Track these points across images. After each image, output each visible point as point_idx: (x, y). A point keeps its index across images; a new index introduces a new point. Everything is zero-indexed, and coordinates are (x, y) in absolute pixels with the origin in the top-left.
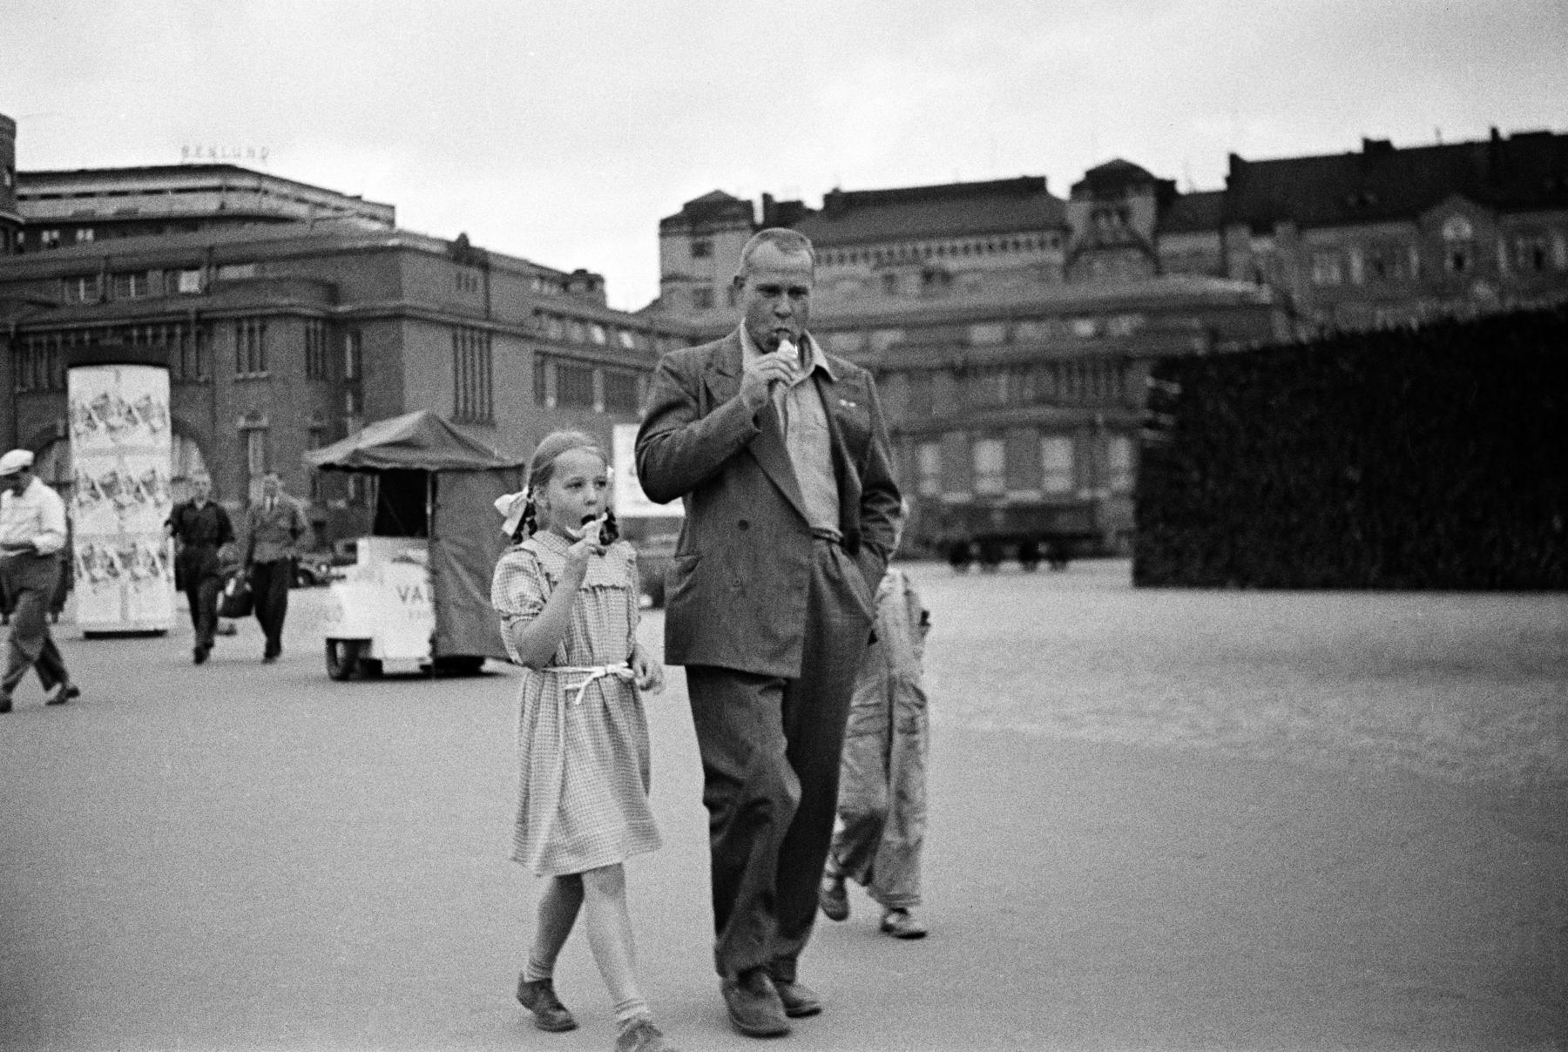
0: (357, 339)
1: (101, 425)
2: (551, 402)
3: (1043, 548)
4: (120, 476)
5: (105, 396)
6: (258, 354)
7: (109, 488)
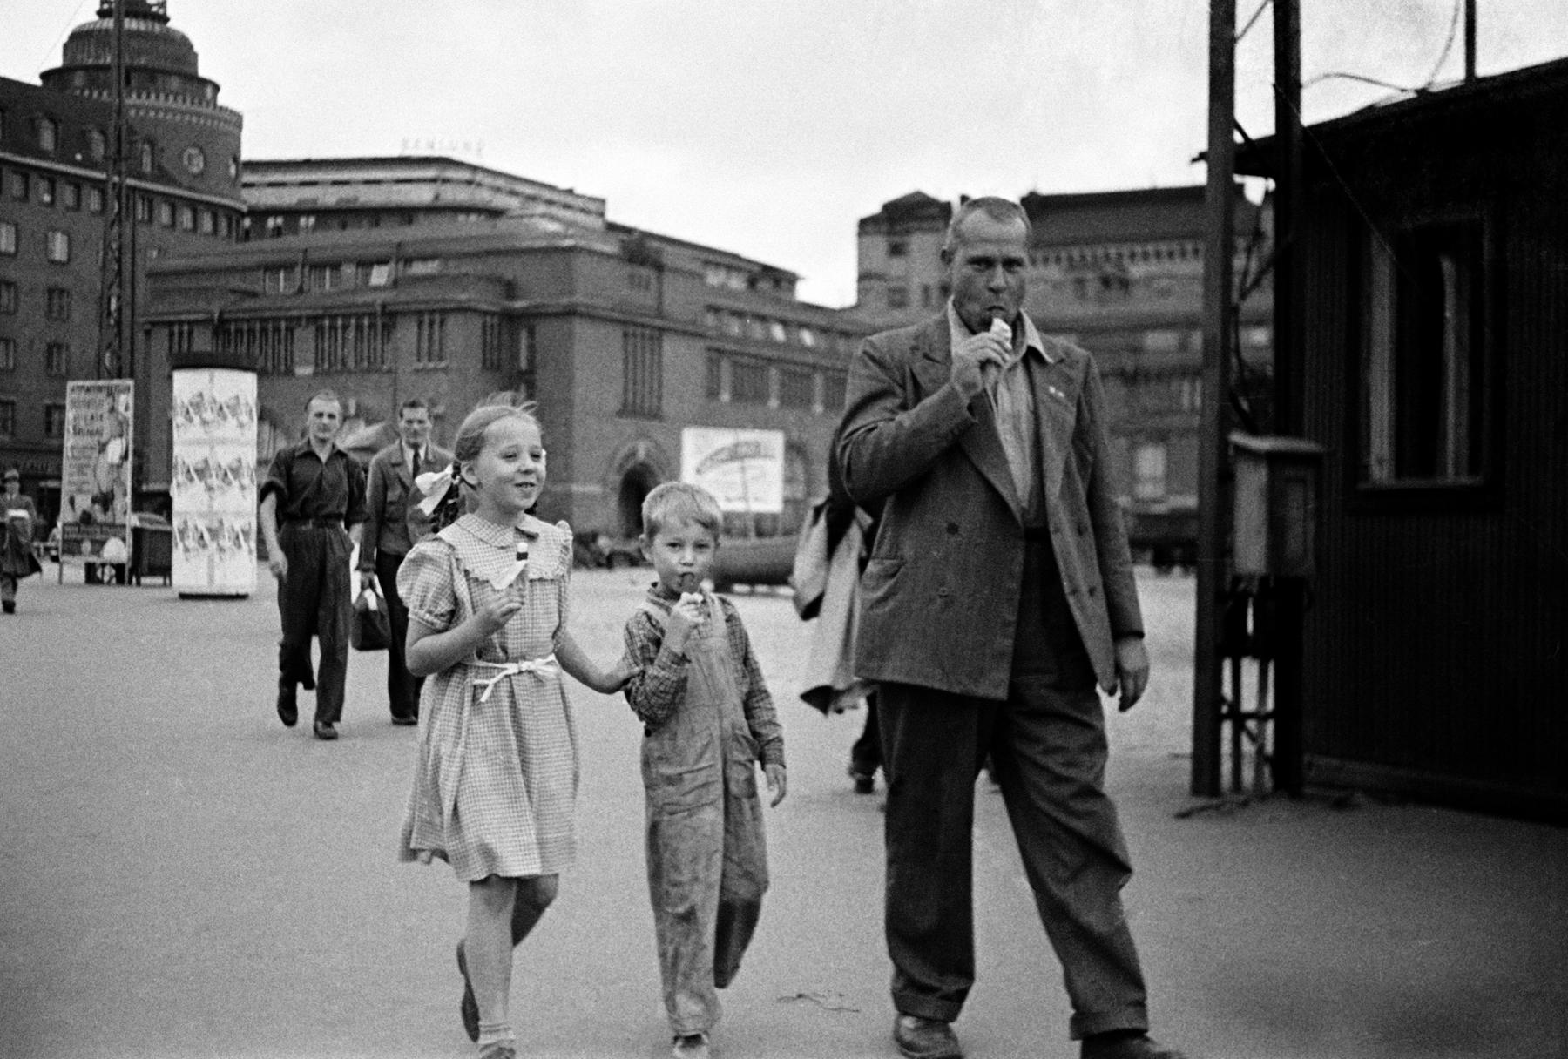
0: (532, 333)
1: (197, 419)
2: (725, 397)
3: (1178, 553)
4: (211, 463)
5: (201, 395)
6: (437, 343)
7: (202, 473)
